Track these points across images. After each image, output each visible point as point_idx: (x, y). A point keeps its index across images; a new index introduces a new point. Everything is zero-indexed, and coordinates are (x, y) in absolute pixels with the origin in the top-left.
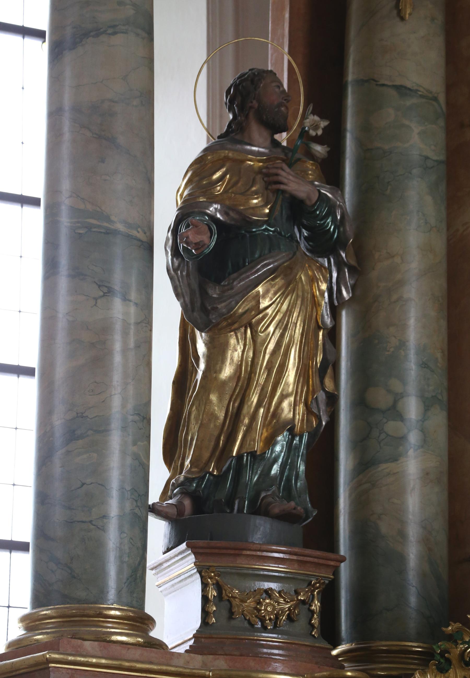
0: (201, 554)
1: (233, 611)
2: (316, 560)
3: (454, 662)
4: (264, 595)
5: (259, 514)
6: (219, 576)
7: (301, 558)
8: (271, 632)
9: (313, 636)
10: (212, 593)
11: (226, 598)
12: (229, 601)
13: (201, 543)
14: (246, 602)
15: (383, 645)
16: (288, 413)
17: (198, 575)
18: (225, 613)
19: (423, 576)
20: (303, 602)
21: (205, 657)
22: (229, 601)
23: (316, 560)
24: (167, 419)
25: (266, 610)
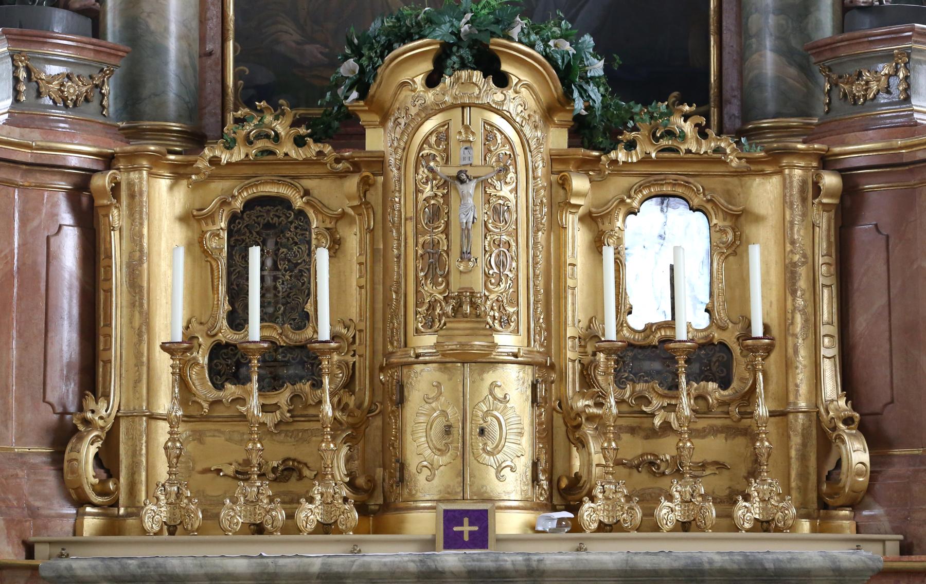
0: (13, 40)
1: (41, 91)
2: (108, 50)
3: (239, 140)
4: (66, 79)
5: (58, 7)
6: (29, 60)
7: (98, 48)
8: (59, 108)
9: (104, 115)
10: (22, 74)
11: (35, 79)
12: (36, 82)
13: (15, 30)
14: (51, 84)
15: (146, 124)
16: (786, 356)
17: (10, 60)
18: (34, 94)
19: (182, 67)
20: (96, 86)
21: (22, 130)
22: (36, 82)
23: (108, 50)
24: (752, 300)
25: (68, 91)
